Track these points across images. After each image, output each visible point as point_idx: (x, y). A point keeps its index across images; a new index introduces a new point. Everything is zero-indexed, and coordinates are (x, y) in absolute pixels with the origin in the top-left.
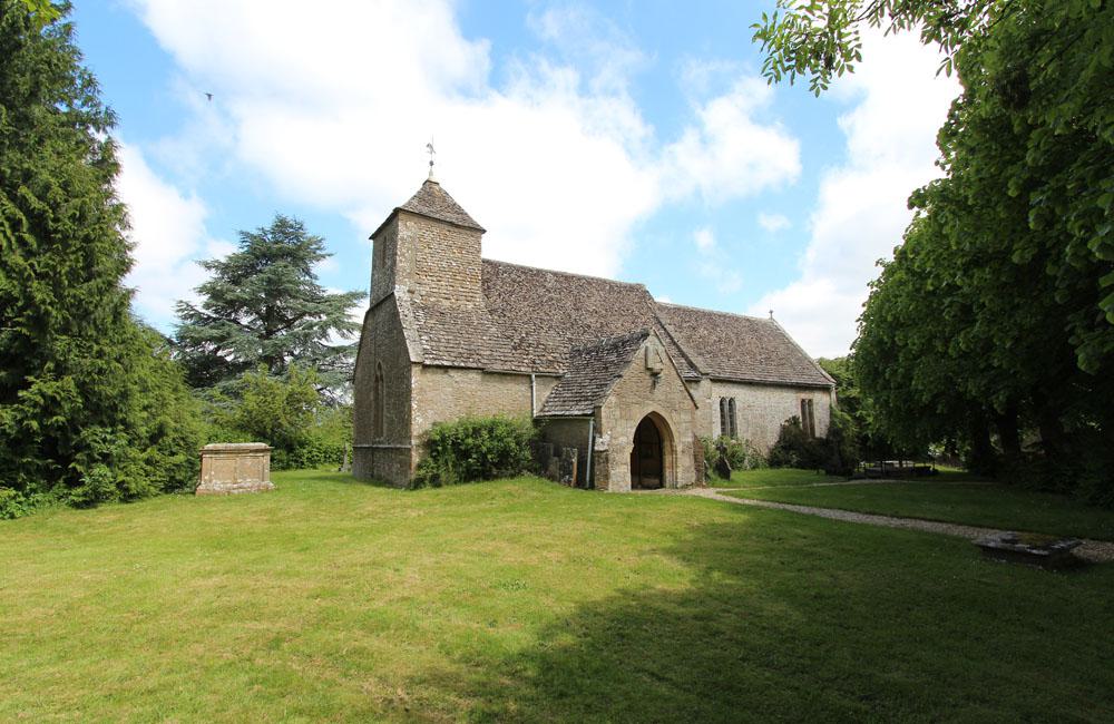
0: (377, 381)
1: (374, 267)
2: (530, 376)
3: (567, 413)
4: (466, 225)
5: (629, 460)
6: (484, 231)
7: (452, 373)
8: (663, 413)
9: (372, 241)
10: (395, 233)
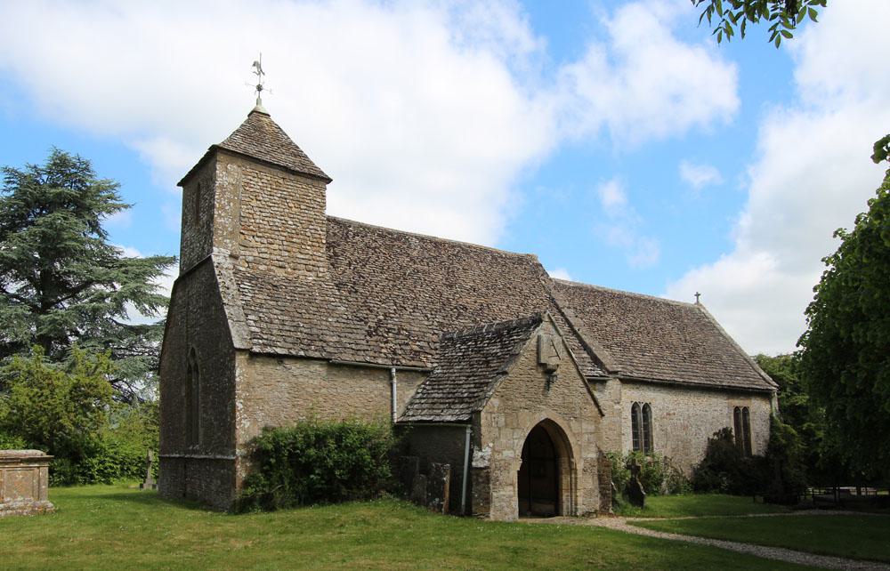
0: (189, 372)
1: (184, 222)
2: (390, 370)
3: (438, 419)
4: (306, 171)
5: (516, 480)
6: (329, 180)
7: (288, 364)
8: (560, 422)
9: (181, 188)
10: (212, 179)
